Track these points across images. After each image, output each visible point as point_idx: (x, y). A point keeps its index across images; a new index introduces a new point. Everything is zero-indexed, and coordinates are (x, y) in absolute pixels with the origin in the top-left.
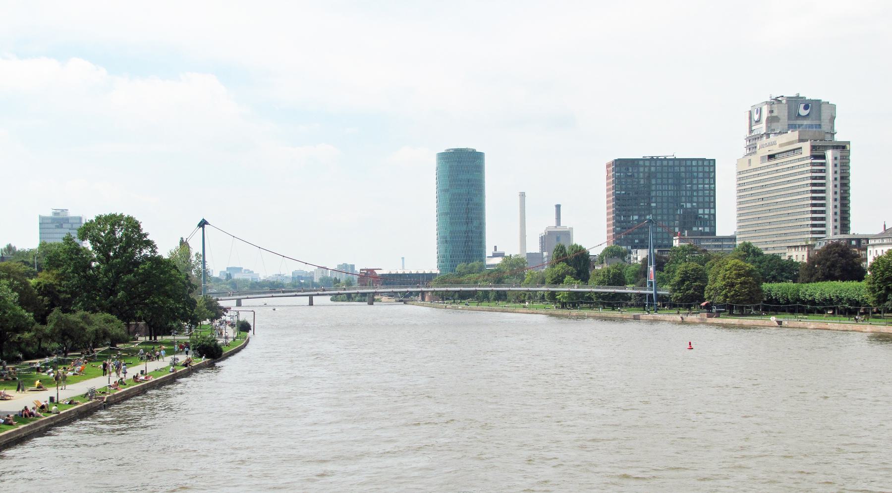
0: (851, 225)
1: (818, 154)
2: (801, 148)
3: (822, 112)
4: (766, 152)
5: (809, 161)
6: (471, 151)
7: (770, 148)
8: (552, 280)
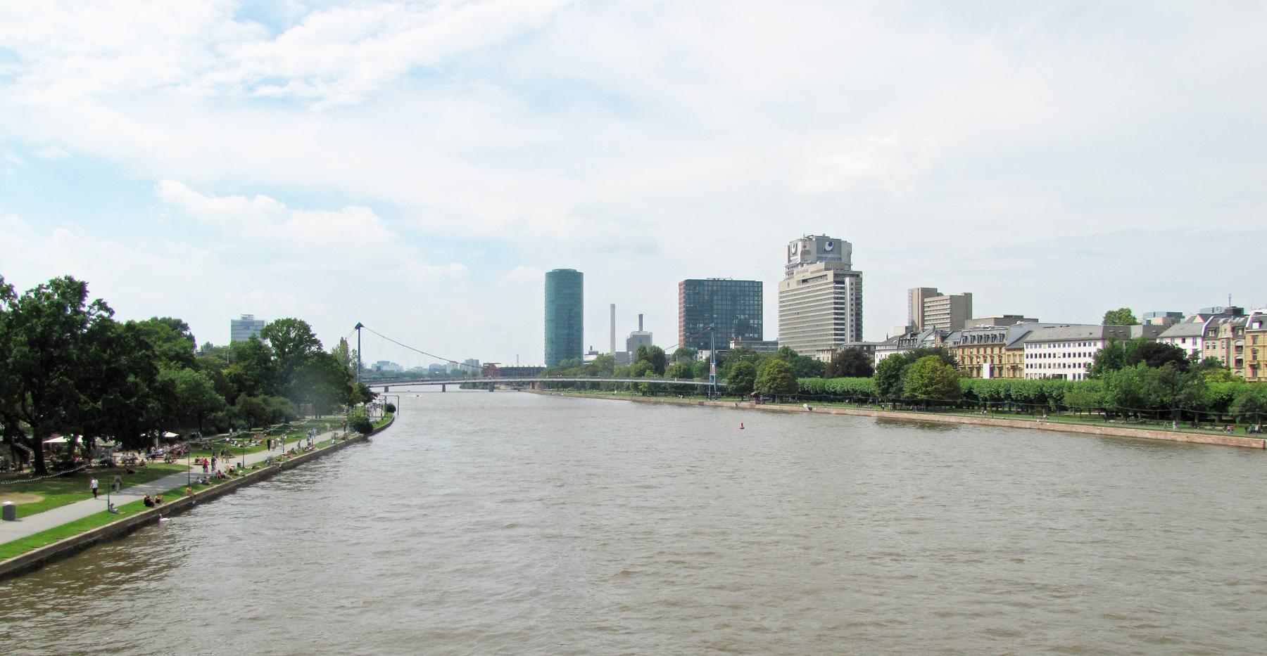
1: (839, 280)
5: (833, 285)
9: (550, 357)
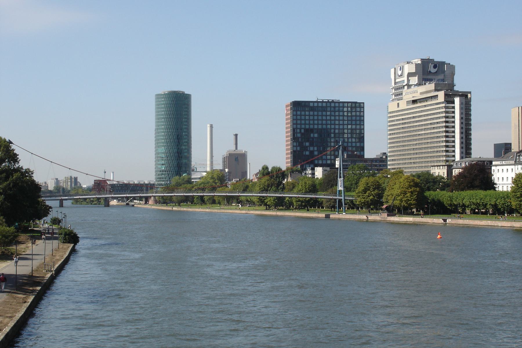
0: (472, 151)
1: (449, 99)
2: (437, 95)
3: (422, 69)
4: (410, 98)
5: (444, 105)
6: (181, 93)
7: (414, 95)
8: (260, 189)
9: (159, 173)
